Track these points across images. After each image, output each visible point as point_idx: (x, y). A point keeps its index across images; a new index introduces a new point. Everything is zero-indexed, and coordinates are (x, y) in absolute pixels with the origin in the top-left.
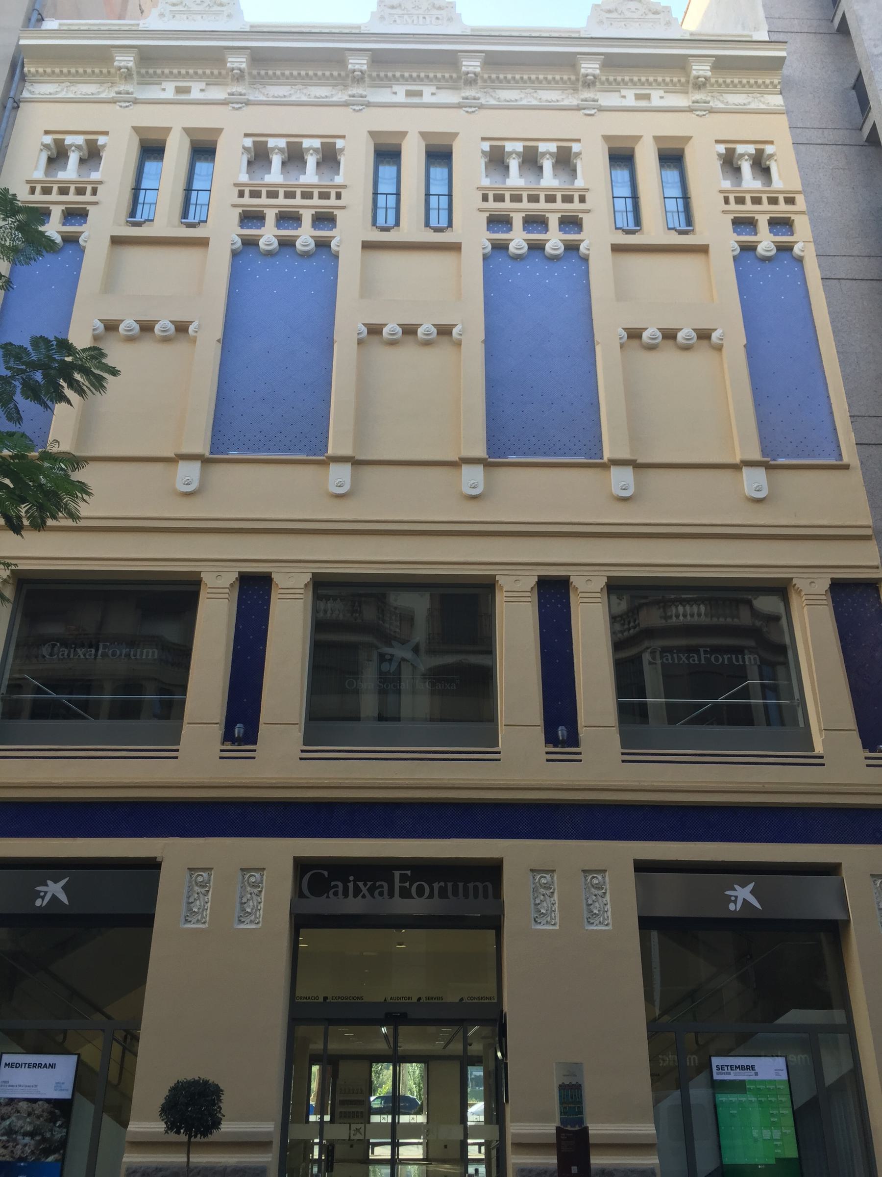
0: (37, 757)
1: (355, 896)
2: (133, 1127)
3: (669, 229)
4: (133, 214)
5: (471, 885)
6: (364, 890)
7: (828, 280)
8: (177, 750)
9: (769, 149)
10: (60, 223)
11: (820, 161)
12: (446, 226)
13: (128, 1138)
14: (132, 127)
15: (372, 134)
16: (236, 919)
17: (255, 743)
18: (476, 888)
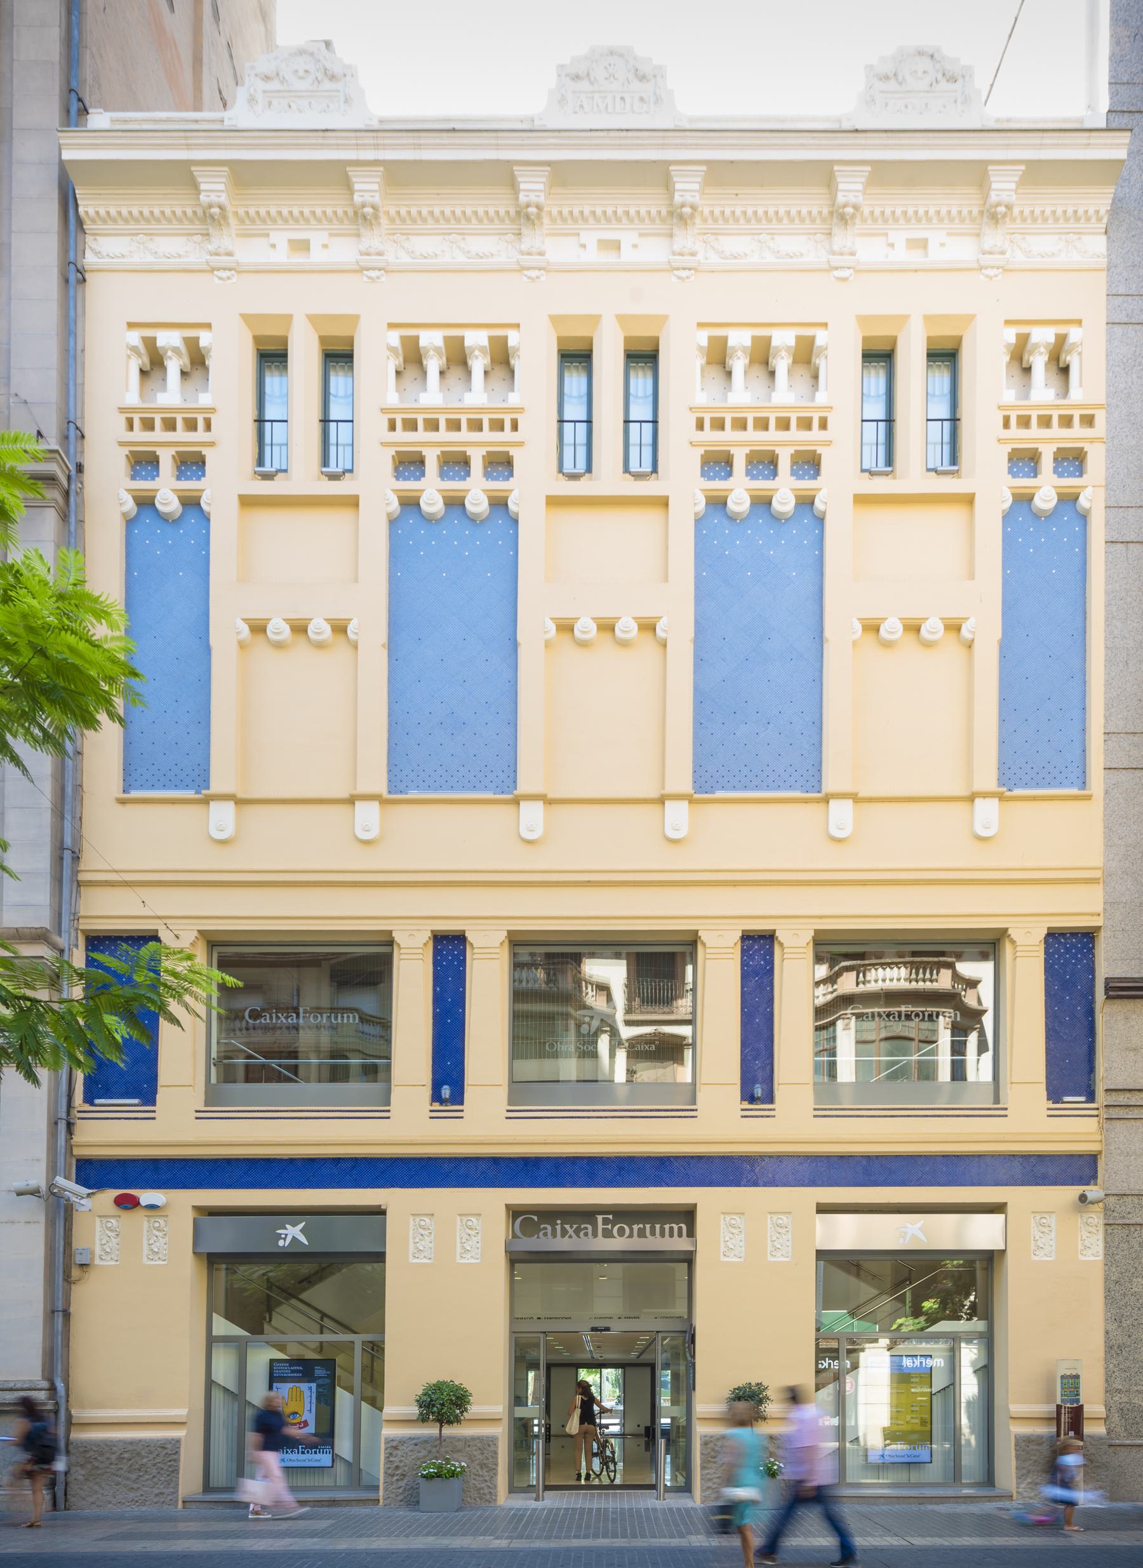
0: (939, 1116)
1: (563, 1236)
2: (386, 1410)
3: (928, 470)
4: (260, 462)
5: (667, 1227)
6: (571, 1231)
7: (1113, 545)
8: (389, 1111)
9: (821, 338)
10: (172, 476)
11: (1138, 353)
12: (583, 471)
13: (384, 1417)
14: (241, 315)
15: (247, 318)
16: (458, 1256)
17: (462, 1103)
18: (671, 1229)
